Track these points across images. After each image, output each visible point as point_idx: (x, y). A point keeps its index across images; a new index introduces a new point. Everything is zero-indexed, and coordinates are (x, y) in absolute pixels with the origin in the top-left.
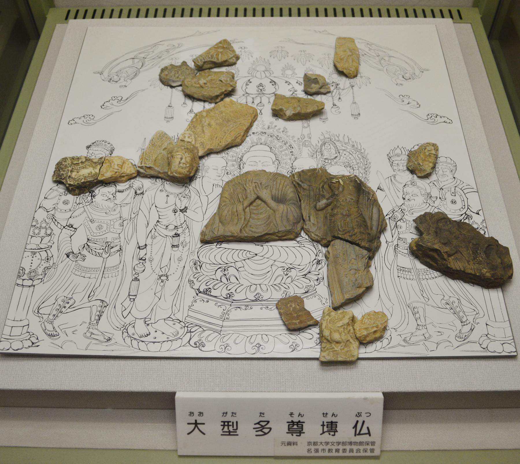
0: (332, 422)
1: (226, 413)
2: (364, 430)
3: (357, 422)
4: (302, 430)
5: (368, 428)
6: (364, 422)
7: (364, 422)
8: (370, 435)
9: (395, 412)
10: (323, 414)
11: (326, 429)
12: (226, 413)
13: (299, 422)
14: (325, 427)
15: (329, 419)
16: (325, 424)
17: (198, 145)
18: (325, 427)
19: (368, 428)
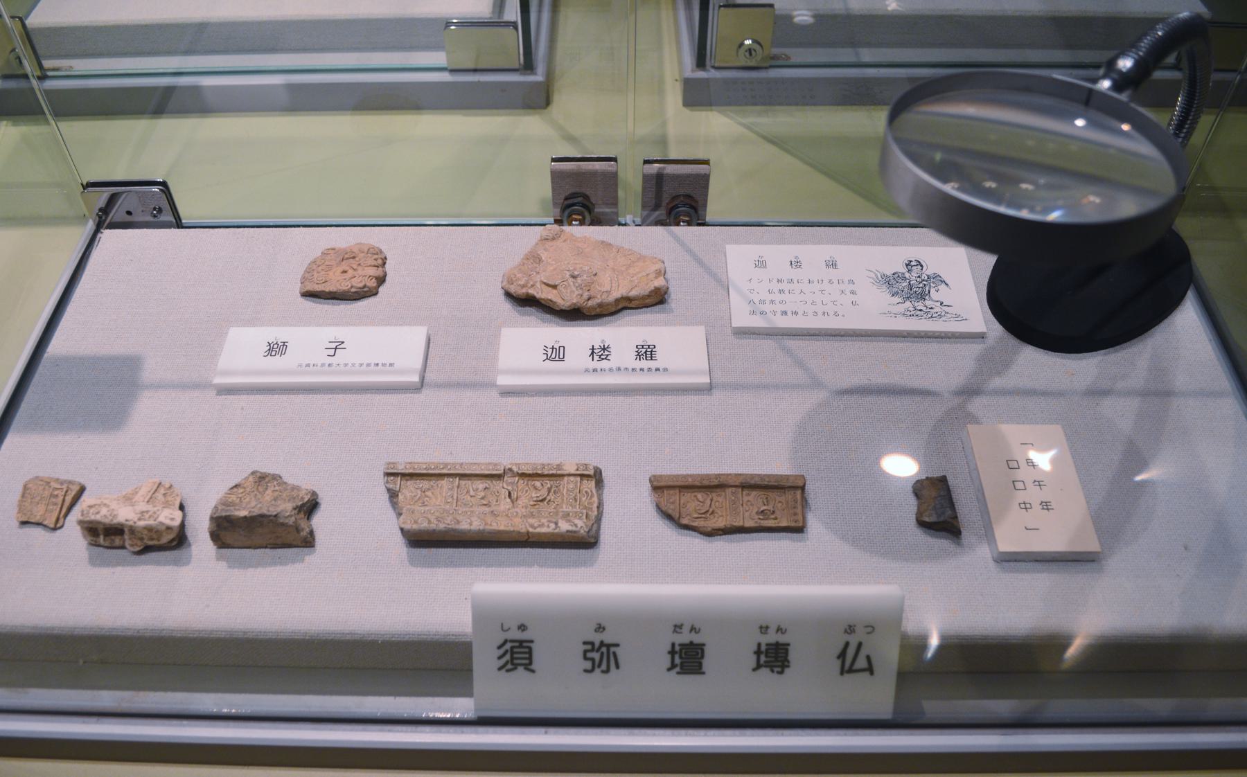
0: (777, 644)
1: (767, 627)
2: (861, 663)
3: (847, 644)
4: (531, 663)
5: (868, 658)
6: (860, 645)
7: (860, 645)
8: (872, 673)
9: (904, 622)
10: (761, 627)
11: (763, 658)
12: (767, 627)
13: (602, 644)
14: (677, 657)
15: (772, 637)
16: (677, 648)
17: (928, 303)
18: (677, 657)
19: (868, 658)
